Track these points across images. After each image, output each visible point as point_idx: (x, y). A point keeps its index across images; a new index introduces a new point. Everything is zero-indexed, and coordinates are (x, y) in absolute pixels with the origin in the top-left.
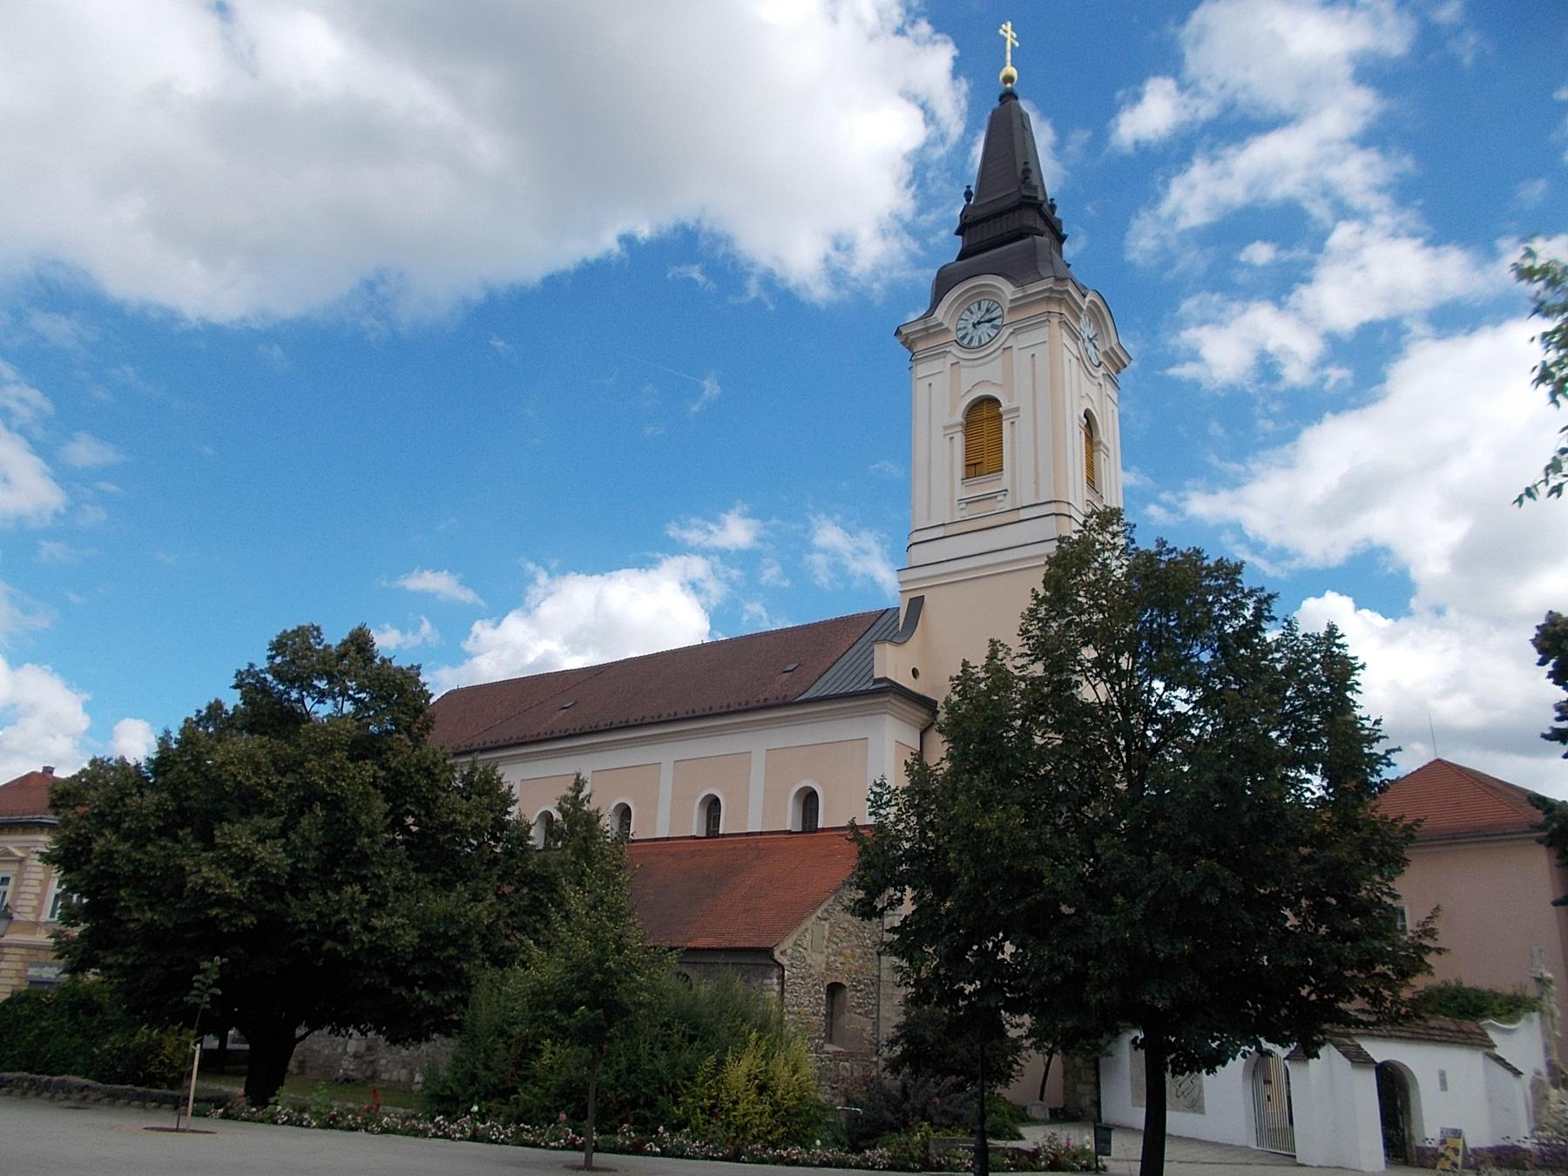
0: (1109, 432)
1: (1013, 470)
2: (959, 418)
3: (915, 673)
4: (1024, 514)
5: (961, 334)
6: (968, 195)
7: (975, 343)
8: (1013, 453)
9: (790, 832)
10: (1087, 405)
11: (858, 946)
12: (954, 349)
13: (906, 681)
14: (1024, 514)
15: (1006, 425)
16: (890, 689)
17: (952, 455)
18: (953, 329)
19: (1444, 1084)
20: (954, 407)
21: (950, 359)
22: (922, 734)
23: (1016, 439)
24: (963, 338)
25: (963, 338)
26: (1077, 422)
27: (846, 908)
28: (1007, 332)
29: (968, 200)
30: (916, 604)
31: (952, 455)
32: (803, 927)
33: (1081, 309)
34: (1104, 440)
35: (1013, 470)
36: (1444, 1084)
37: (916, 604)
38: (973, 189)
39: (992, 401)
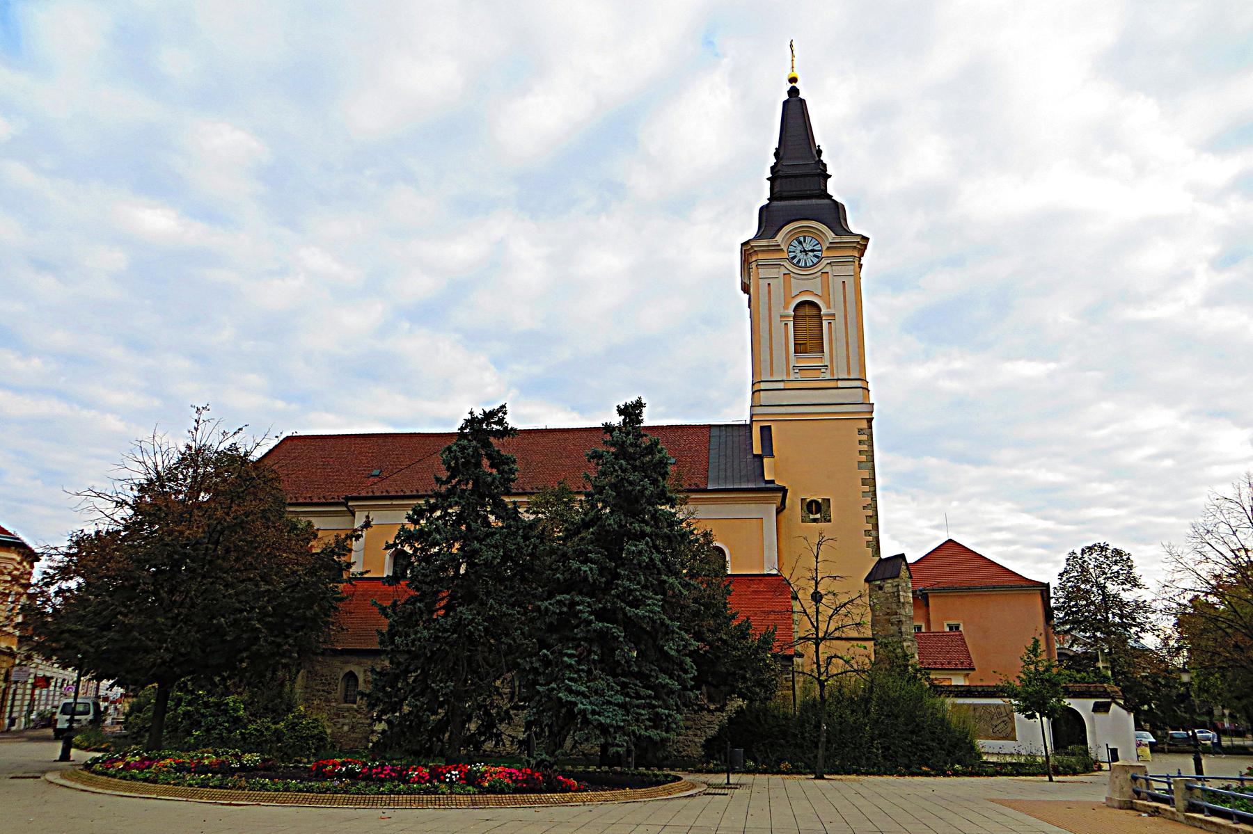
4: (840, 384)
5: (791, 255)
12: (786, 264)
14: (840, 384)
24: (794, 258)
25: (794, 258)
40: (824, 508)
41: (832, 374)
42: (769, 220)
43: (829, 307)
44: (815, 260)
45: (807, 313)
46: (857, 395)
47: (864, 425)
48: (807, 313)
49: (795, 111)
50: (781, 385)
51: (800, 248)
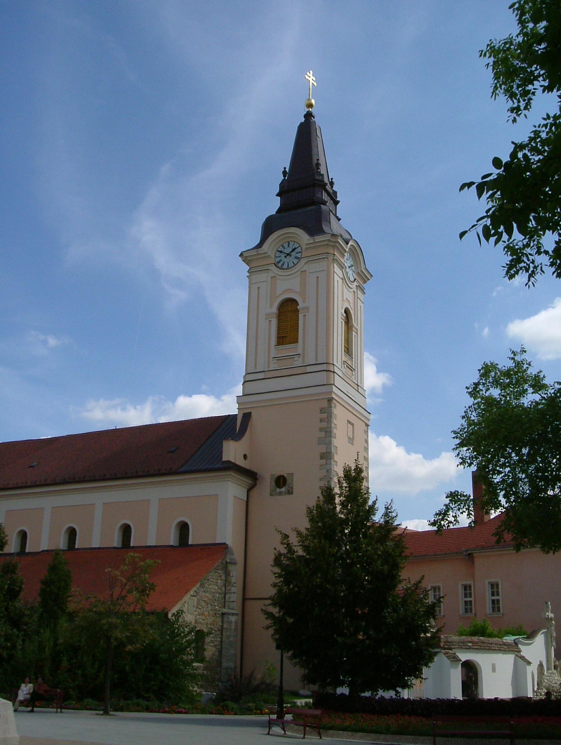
0: (362, 307)
1: (304, 343)
2: (274, 310)
3: (245, 457)
4: (309, 369)
5: (277, 260)
6: (284, 173)
7: (285, 266)
8: (304, 330)
9: (172, 546)
10: (346, 305)
11: (212, 610)
12: (273, 268)
13: (240, 462)
14: (309, 369)
15: (301, 316)
16: (231, 467)
17: (270, 334)
18: (273, 256)
19: (494, 670)
20: (271, 306)
21: (271, 274)
22: (248, 491)
23: (306, 324)
24: (279, 262)
25: (279, 262)
26: (340, 316)
27: (533, 393)
28: (303, 261)
29: (284, 176)
30: (247, 417)
31: (270, 334)
32: (183, 601)
33: (345, 251)
34: (355, 325)
35: (304, 343)
36: (494, 670)
37: (247, 417)
38: (287, 170)
39: (294, 302)
40: (289, 481)
41: (303, 361)
42: (270, 227)
43: (304, 301)
44: (296, 261)
45: (288, 311)
46: (320, 378)
47: (325, 404)
48: (288, 311)
49: (306, 134)
50: (261, 376)
51: (283, 255)
